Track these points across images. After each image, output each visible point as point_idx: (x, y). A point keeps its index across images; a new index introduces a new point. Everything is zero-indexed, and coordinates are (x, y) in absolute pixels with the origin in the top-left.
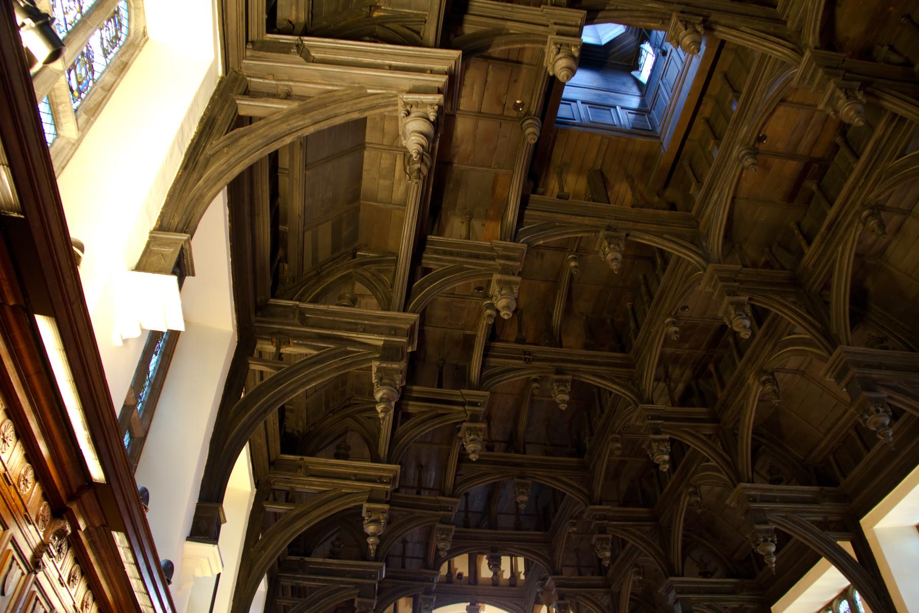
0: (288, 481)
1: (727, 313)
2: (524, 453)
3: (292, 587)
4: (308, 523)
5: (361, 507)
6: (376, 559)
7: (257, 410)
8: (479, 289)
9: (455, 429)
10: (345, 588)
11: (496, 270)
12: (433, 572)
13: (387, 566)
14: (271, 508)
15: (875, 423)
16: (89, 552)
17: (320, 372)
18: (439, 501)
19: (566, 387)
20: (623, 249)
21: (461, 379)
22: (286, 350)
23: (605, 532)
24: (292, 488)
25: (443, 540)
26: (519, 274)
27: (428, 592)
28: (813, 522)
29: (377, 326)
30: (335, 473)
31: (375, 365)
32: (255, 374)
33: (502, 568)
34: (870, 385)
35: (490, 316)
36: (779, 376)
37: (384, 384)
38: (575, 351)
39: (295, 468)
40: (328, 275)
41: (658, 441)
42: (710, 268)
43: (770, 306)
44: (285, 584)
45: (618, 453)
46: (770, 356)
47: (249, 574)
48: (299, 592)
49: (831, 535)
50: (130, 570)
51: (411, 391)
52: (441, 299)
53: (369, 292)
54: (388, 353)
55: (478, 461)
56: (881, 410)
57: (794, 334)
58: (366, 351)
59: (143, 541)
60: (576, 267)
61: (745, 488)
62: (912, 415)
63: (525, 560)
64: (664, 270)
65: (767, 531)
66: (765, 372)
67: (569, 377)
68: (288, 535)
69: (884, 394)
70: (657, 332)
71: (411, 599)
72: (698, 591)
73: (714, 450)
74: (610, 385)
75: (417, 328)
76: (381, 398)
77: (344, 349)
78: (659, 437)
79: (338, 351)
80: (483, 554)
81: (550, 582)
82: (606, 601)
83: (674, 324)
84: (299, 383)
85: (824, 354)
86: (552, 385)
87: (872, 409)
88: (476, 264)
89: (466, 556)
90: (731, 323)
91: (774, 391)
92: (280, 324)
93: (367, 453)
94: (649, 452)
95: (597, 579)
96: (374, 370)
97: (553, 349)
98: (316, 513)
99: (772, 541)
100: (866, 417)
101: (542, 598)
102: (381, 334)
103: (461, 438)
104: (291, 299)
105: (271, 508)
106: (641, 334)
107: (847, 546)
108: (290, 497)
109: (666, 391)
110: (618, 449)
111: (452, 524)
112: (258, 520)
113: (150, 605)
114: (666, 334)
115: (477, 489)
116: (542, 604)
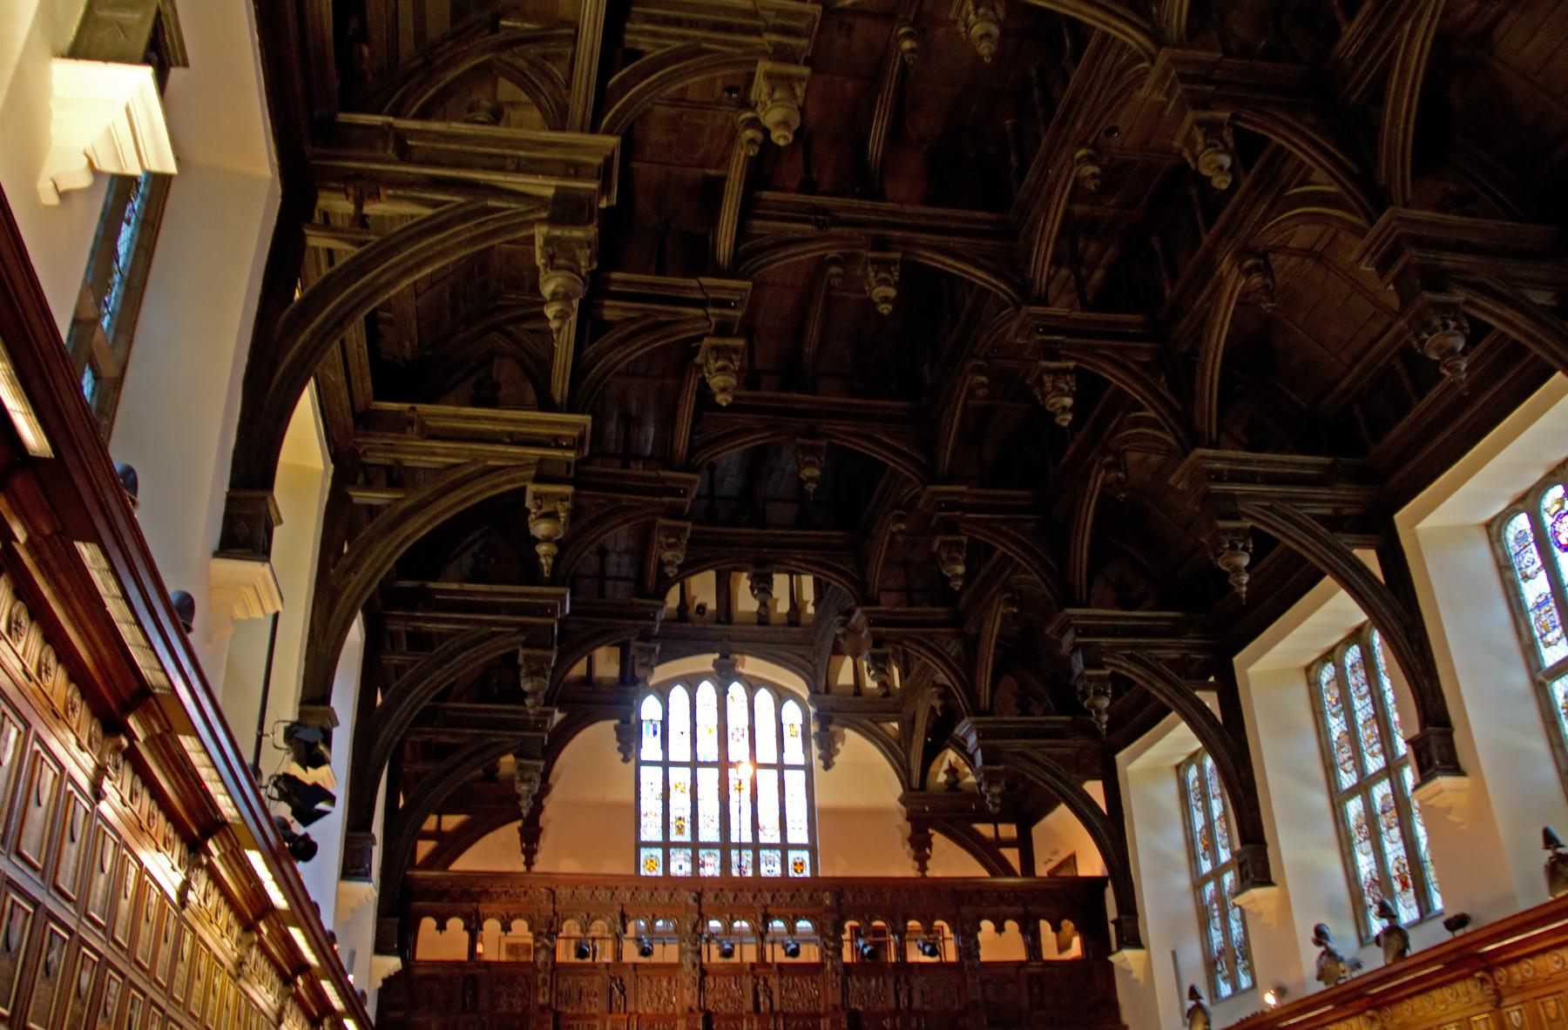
0: (390, 449)
1: (1189, 141)
2: (814, 393)
3: (407, 633)
4: (429, 522)
5: (523, 490)
6: (553, 582)
7: (326, 321)
8: (730, 89)
9: (687, 350)
10: (500, 633)
11: (764, 53)
12: (655, 602)
13: (572, 595)
14: (361, 497)
15: (1439, 348)
16: (39, 580)
17: (439, 248)
18: (662, 480)
19: (891, 273)
20: (1001, 16)
21: (699, 258)
22: (371, 209)
23: (956, 532)
24: (398, 461)
25: (670, 546)
26: (807, 62)
27: (646, 636)
28: (1315, 517)
29: (542, 161)
30: (475, 432)
31: (540, 232)
32: (317, 256)
33: (775, 593)
34: (1436, 279)
35: (752, 141)
36: (1277, 261)
37: (559, 268)
38: (910, 209)
39: (400, 424)
40: (447, 66)
42: (1163, 57)
43: (1270, 130)
44: (393, 628)
45: (981, 392)
46: (1263, 224)
47: (330, 614)
48: (420, 641)
49: (1344, 540)
50: (116, 608)
51: (608, 281)
52: (660, 111)
53: (524, 98)
54: (566, 209)
55: (731, 408)
56: (1452, 324)
57: (1312, 183)
58: (521, 207)
59: (133, 558)
60: (912, 50)
61: (1202, 457)
62: (1503, 334)
63: (815, 580)
64: (1076, 58)
65: (1236, 531)
66: (1252, 252)
67: (897, 255)
68: (396, 543)
69: (1460, 296)
70: (1058, 176)
71: (617, 650)
72: (1113, 632)
73: (1154, 392)
74: (972, 270)
75: (616, 162)
76: (554, 295)
77: (481, 204)
79: (470, 208)
80: (741, 570)
81: (858, 617)
82: (954, 648)
83: (1090, 159)
84: (400, 269)
85: (1361, 222)
86: (865, 269)
87: (1437, 322)
88: (726, 43)
89: (711, 575)
90: (1196, 159)
91: (1266, 286)
92: (359, 159)
93: (530, 395)
94: (1036, 391)
95: (941, 611)
96: (539, 241)
97: (867, 204)
98: (444, 503)
99: (1245, 549)
100: (1425, 336)
101: (845, 644)
102: (551, 174)
103: (700, 367)
104: (378, 112)
105: (361, 497)
106: (1030, 178)
107: (1369, 558)
108: (396, 477)
109: (1072, 284)
110: (982, 385)
111: (686, 519)
112: (341, 522)
113: (157, 666)
114: (1076, 179)
115: (730, 457)
116: (844, 654)
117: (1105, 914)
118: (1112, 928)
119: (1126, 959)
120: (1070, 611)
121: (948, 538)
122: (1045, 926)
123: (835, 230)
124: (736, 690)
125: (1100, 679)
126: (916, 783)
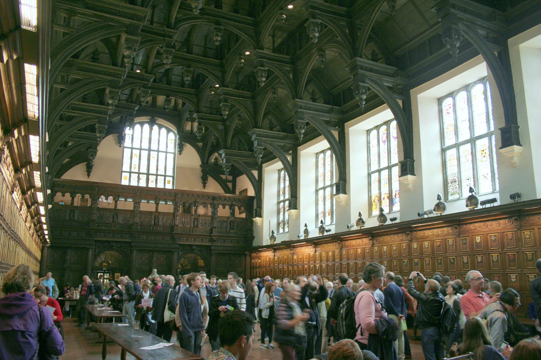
41: (262, 70)
70: (273, 14)
72: (267, 136)
78: (262, 68)
117: (253, 207)
118: (254, 211)
119: (257, 220)
120: (255, 129)
121: (225, 103)
122: (236, 208)
123: (205, 16)
124: (156, 127)
125: (261, 149)
126: (205, 162)
